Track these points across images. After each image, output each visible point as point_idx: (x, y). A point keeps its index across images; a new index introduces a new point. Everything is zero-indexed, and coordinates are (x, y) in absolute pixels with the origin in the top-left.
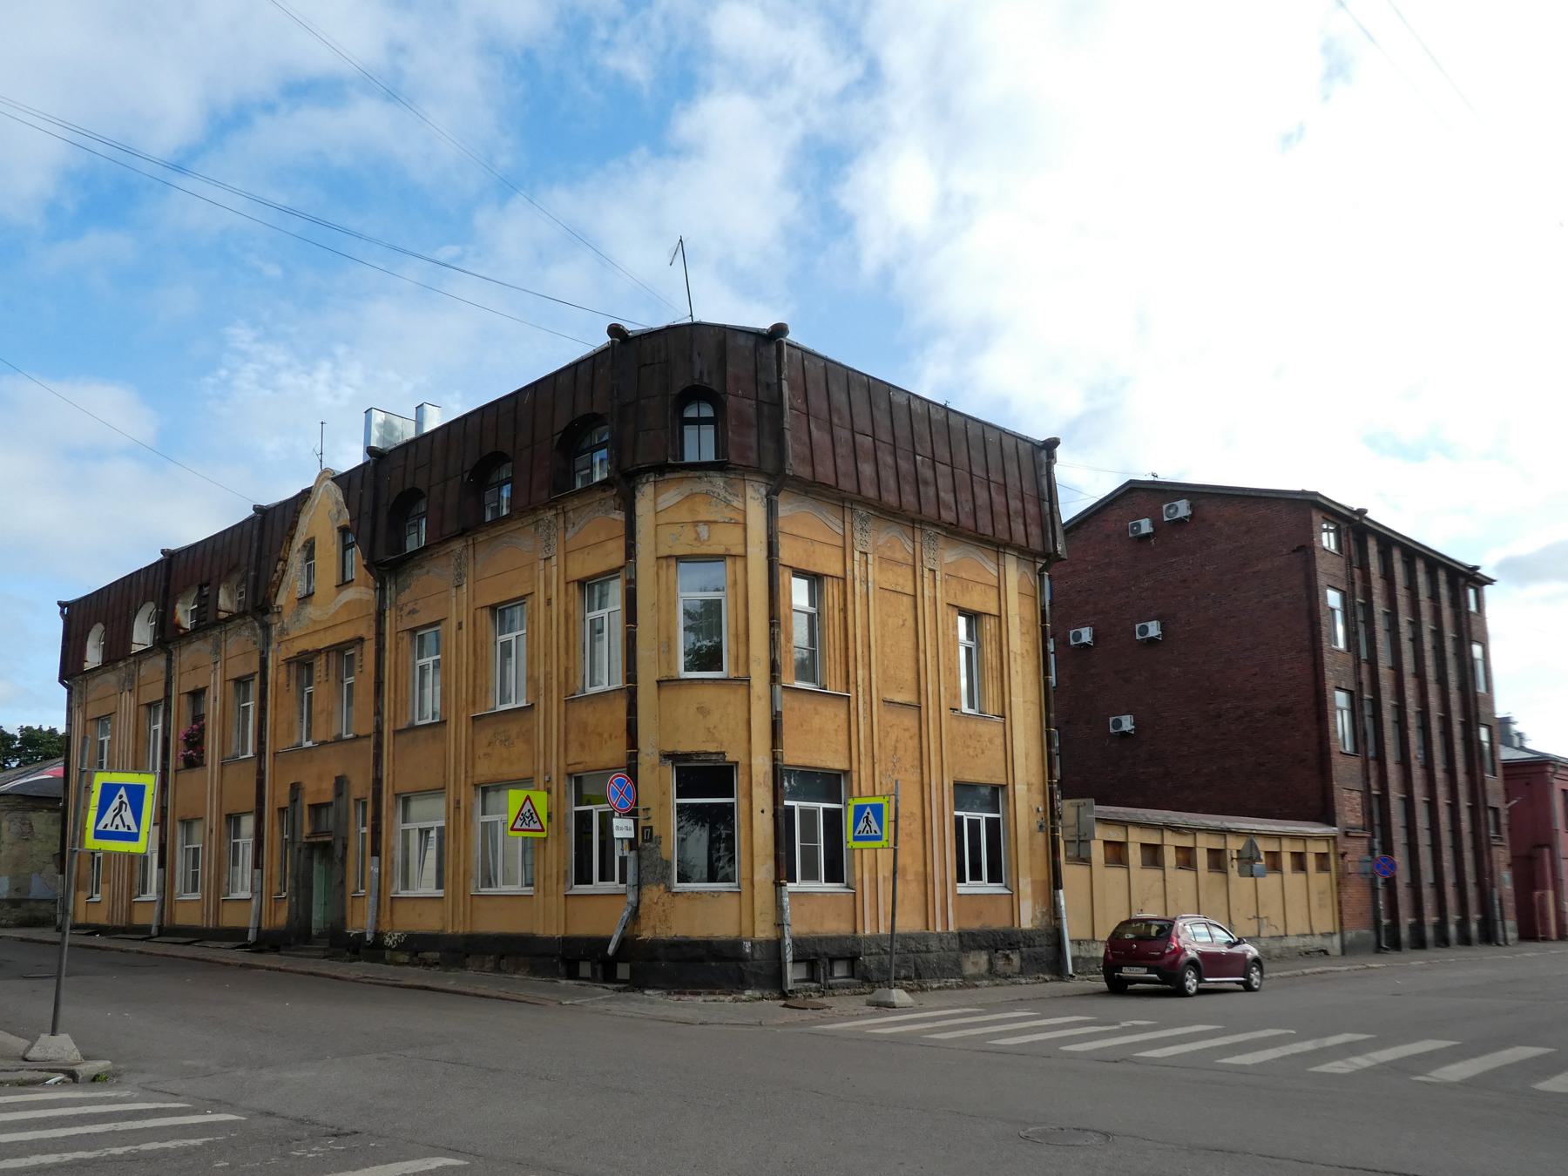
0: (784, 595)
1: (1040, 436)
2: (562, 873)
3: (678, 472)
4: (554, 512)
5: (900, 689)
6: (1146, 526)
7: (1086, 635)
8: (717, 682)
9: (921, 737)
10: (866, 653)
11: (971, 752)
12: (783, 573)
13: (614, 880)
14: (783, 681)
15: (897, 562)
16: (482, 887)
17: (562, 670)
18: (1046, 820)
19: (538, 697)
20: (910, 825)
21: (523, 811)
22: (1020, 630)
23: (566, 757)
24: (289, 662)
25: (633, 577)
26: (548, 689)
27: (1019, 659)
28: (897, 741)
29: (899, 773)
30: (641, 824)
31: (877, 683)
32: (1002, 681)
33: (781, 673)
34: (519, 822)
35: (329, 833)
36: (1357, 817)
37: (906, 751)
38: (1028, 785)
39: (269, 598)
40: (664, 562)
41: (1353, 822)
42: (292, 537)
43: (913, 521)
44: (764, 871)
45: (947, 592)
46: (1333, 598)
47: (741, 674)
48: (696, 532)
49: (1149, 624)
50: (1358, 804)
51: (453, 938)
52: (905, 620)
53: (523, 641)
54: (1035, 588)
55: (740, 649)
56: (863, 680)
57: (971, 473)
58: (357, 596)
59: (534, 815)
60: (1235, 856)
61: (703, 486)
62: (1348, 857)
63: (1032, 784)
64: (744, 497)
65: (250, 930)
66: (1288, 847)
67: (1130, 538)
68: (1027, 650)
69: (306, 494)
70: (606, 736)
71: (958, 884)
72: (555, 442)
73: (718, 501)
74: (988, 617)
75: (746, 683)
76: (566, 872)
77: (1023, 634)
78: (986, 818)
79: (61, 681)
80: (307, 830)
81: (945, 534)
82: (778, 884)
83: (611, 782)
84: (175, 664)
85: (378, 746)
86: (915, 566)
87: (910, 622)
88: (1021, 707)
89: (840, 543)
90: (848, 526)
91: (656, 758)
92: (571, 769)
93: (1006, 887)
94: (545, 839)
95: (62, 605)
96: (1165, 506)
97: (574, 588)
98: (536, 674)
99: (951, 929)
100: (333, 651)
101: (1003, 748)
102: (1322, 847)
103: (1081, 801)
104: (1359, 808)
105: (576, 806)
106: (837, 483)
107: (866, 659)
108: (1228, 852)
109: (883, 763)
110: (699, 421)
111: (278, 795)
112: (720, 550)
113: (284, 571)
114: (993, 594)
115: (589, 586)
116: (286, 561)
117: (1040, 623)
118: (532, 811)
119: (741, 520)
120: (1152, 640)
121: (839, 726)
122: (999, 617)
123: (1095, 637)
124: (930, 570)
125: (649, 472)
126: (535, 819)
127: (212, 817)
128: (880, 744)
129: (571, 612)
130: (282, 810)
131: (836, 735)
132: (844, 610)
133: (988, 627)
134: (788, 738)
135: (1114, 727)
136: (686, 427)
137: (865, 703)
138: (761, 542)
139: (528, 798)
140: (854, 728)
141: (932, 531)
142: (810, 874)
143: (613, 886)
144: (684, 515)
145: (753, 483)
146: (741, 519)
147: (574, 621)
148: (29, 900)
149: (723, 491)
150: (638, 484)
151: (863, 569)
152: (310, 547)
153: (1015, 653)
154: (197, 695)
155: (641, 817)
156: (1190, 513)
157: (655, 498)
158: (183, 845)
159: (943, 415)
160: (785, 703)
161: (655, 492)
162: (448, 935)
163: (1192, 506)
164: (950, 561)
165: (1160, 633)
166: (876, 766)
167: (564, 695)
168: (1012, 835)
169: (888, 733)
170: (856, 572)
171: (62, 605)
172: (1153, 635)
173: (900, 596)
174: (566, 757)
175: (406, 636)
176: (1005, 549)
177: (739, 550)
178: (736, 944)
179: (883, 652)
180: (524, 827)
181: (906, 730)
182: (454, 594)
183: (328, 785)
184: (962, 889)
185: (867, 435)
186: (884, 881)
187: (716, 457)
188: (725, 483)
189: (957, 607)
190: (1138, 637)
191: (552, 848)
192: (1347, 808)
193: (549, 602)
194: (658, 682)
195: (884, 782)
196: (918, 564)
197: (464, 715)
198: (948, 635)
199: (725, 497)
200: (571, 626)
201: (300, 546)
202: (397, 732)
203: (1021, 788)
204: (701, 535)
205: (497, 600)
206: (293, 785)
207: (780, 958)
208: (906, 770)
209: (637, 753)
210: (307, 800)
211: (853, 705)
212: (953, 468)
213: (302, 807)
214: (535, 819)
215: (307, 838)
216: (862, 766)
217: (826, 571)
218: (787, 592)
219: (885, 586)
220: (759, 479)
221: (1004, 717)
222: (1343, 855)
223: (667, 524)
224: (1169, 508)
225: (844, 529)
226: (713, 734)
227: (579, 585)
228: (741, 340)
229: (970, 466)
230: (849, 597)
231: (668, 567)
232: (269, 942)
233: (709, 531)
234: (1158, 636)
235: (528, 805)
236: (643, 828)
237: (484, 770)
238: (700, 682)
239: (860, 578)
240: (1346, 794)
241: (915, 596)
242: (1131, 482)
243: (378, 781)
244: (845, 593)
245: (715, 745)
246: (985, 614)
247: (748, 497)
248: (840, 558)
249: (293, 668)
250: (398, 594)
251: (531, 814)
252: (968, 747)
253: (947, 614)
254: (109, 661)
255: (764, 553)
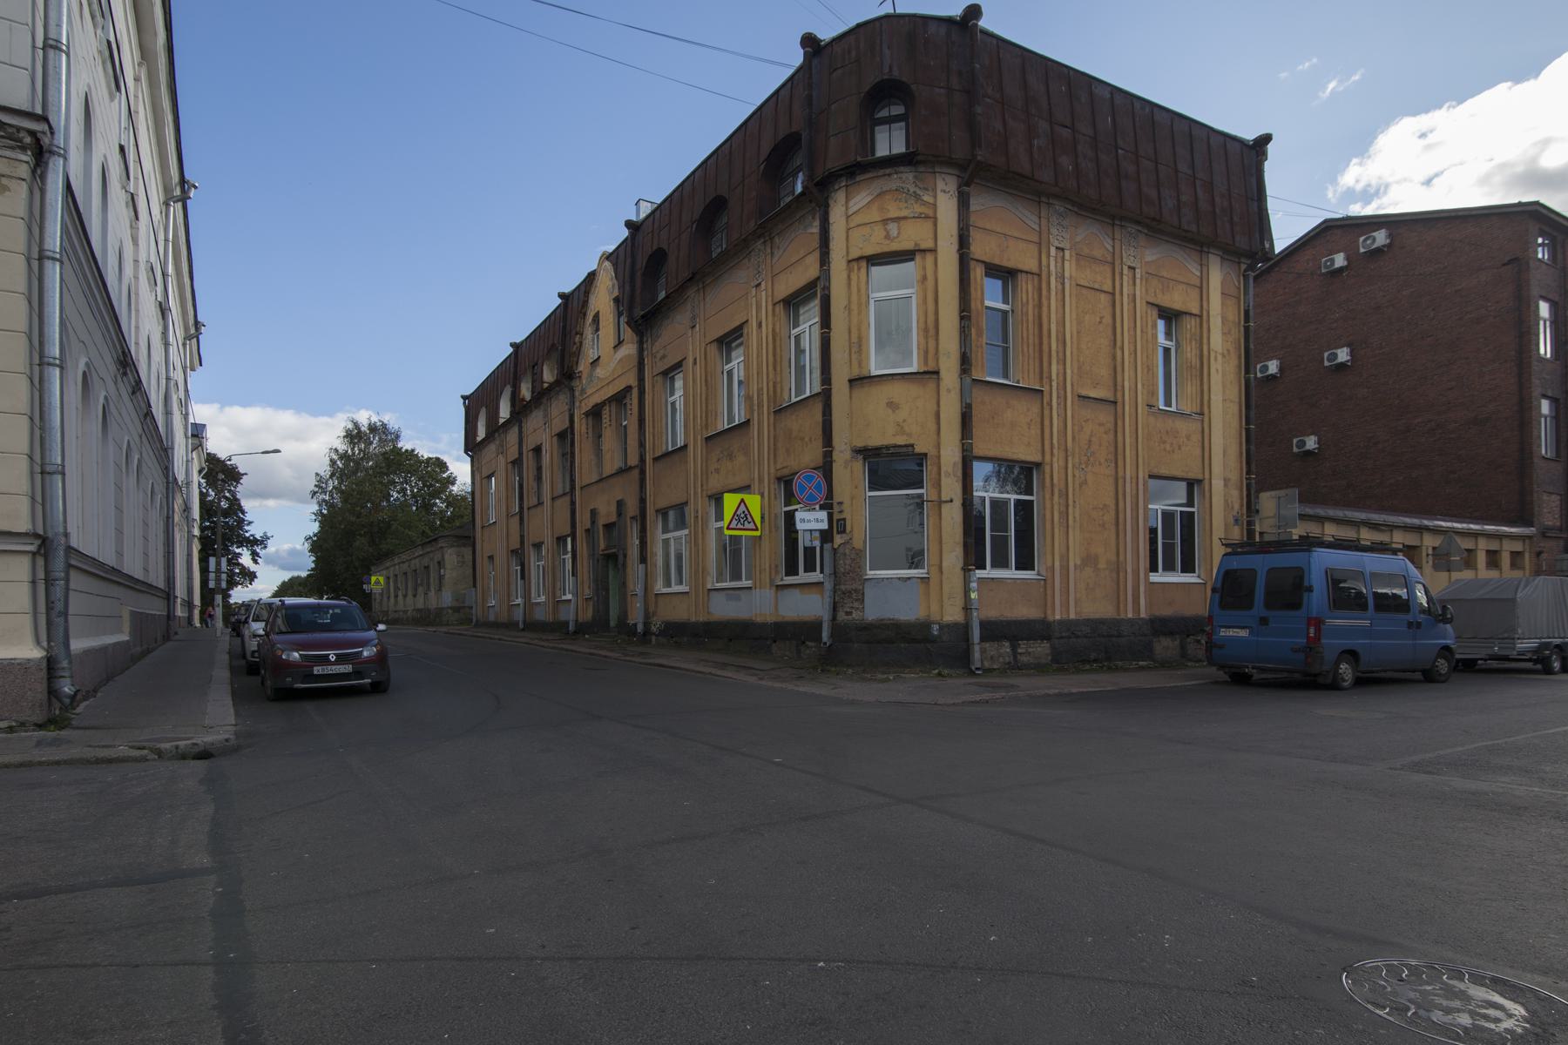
0: (976, 289)
1: (1249, 135)
2: (773, 566)
3: (869, 172)
4: (762, 240)
5: (1095, 385)
6: (1340, 260)
7: (1273, 367)
8: (906, 377)
9: (1116, 432)
10: (1061, 348)
11: (1168, 447)
12: (975, 269)
13: (815, 571)
14: (973, 373)
15: (1095, 259)
16: (717, 582)
17: (771, 384)
18: (1242, 514)
19: (752, 412)
20: (1103, 515)
21: (738, 513)
22: (1222, 330)
23: (775, 462)
24: (587, 414)
25: (827, 284)
26: (760, 405)
27: (1220, 357)
28: (1091, 436)
29: (1093, 465)
30: (836, 517)
31: (1072, 377)
32: (1202, 380)
33: (971, 365)
34: (735, 522)
35: (615, 547)
36: (1555, 518)
37: (1100, 445)
38: (1225, 480)
39: (572, 367)
40: (855, 265)
41: (1550, 523)
42: (585, 314)
43: (1113, 217)
44: (953, 557)
45: (1147, 290)
46: (1544, 309)
47: (931, 367)
48: (886, 229)
49: (1339, 351)
50: (1556, 507)
51: (696, 624)
52: (1101, 318)
53: (742, 365)
54: (1239, 289)
55: (930, 345)
56: (1058, 375)
57: (1177, 171)
58: (627, 352)
59: (748, 516)
60: (1430, 552)
61: (893, 183)
62: (1544, 556)
63: (1229, 480)
64: (934, 190)
65: (571, 623)
66: (1483, 544)
67: (1324, 274)
68: (1228, 351)
69: (591, 277)
70: (807, 439)
71: (1151, 574)
72: (761, 171)
73: (908, 197)
74: (1188, 317)
75: (935, 376)
76: (777, 566)
77: (1224, 334)
78: (1181, 512)
79: (466, 452)
80: (602, 546)
81: (1146, 231)
82: (966, 570)
83: (799, 477)
84: (524, 429)
85: (643, 472)
86: (1113, 264)
87: (1108, 320)
88: (1221, 405)
89: (1036, 239)
90: (1044, 222)
91: (848, 455)
92: (779, 474)
93: (1199, 577)
94: (760, 537)
95: (464, 398)
96: (1362, 239)
97: (780, 309)
98: (751, 393)
99: (1143, 615)
100: (613, 400)
101: (1200, 444)
102: (1518, 547)
103: (1281, 493)
104: (1557, 510)
105: (785, 506)
106: (1033, 176)
107: (1061, 354)
108: (1424, 548)
109: (1077, 456)
110: (890, 120)
111: (583, 521)
112: (909, 246)
113: (581, 343)
114: (1195, 294)
115: (793, 303)
116: (582, 334)
117: (1242, 323)
118: (746, 512)
119: (931, 215)
120: (1342, 365)
121: (1031, 420)
122: (1201, 316)
123: (1281, 369)
124: (1129, 267)
125: (841, 176)
126: (750, 519)
127: (548, 542)
128: (1074, 438)
129: (778, 330)
130: (587, 531)
131: (1029, 428)
132: (1040, 306)
133: (1188, 327)
134: (978, 430)
135: (1297, 446)
136: (877, 128)
137: (1058, 397)
138: (952, 236)
139: (742, 501)
140: (1047, 423)
141: (1132, 228)
142: (1000, 562)
143: (815, 576)
144: (875, 215)
145: (943, 175)
146: (931, 213)
147: (781, 340)
148: (464, 607)
149: (913, 185)
150: (831, 192)
151: (1059, 265)
152: (596, 317)
153: (1216, 352)
154: (537, 450)
155: (836, 508)
156: (1388, 241)
157: (847, 202)
158: (535, 563)
159: (1147, 110)
160: (979, 396)
161: (847, 197)
162: (693, 622)
163: (1390, 236)
164: (1150, 259)
165: (1349, 358)
166: (1070, 459)
167: (772, 408)
168: (1208, 528)
169: (1082, 428)
170: (1052, 267)
171: (464, 398)
172: (1343, 360)
173: (1098, 293)
174: (775, 462)
175: (659, 378)
176: (1208, 248)
177: (929, 244)
178: (925, 625)
179: (1078, 348)
180: (740, 526)
181: (1101, 425)
182: (690, 335)
183: (613, 508)
184: (1155, 578)
185: (1067, 127)
186: (1075, 569)
187: (907, 147)
188: (915, 177)
189: (1157, 306)
190: (1326, 363)
191: (766, 544)
192: (1545, 510)
193: (760, 325)
194: (851, 381)
195: (1077, 475)
196: (1117, 262)
197: (699, 437)
198: (1147, 333)
199: (914, 192)
200: (778, 343)
201: (590, 320)
202: (656, 459)
203: (1217, 485)
204: (891, 233)
205: (721, 333)
206: (592, 510)
207: (968, 640)
208: (1100, 464)
209: (831, 451)
210: (602, 521)
211: (1046, 400)
212: (1157, 163)
213: (598, 529)
214: (750, 519)
215: (603, 551)
216: (1055, 459)
217: (1021, 267)
218: (979, 287)
219: (1082, 283)
220: (950, 171)
221: (1203, 415)
222: (1539, 554)
223: (859, 226)
224: (1365, 240)
225: (1040, 225)
226: (902, 428)
227: (784, 305)
228: (932, 28)
229: (1175, 162)
230: (1044, 292)
231: (859, 269)
232: (581, 629)
233: (899, 228)
234: (1348, 361)
235: (742, 508)
236: (838, 520)
237: (715, 483)
238: (890, 378)
239: (1056, 274)
240: (1545, 497)
241: (1113, 294)
242: (1326, 221)
243: (643, 501)
244: (1040, 289)
245: (905, 437)
246: (1186, 313)
247: (938, 192)
248: (1036, 254)
249: (590, 418)
250: (652, 345)
251: (746, 515)
252: (1164, 442)
253: (1146, 313)
254: (490, 436)
255: (955, 247)
